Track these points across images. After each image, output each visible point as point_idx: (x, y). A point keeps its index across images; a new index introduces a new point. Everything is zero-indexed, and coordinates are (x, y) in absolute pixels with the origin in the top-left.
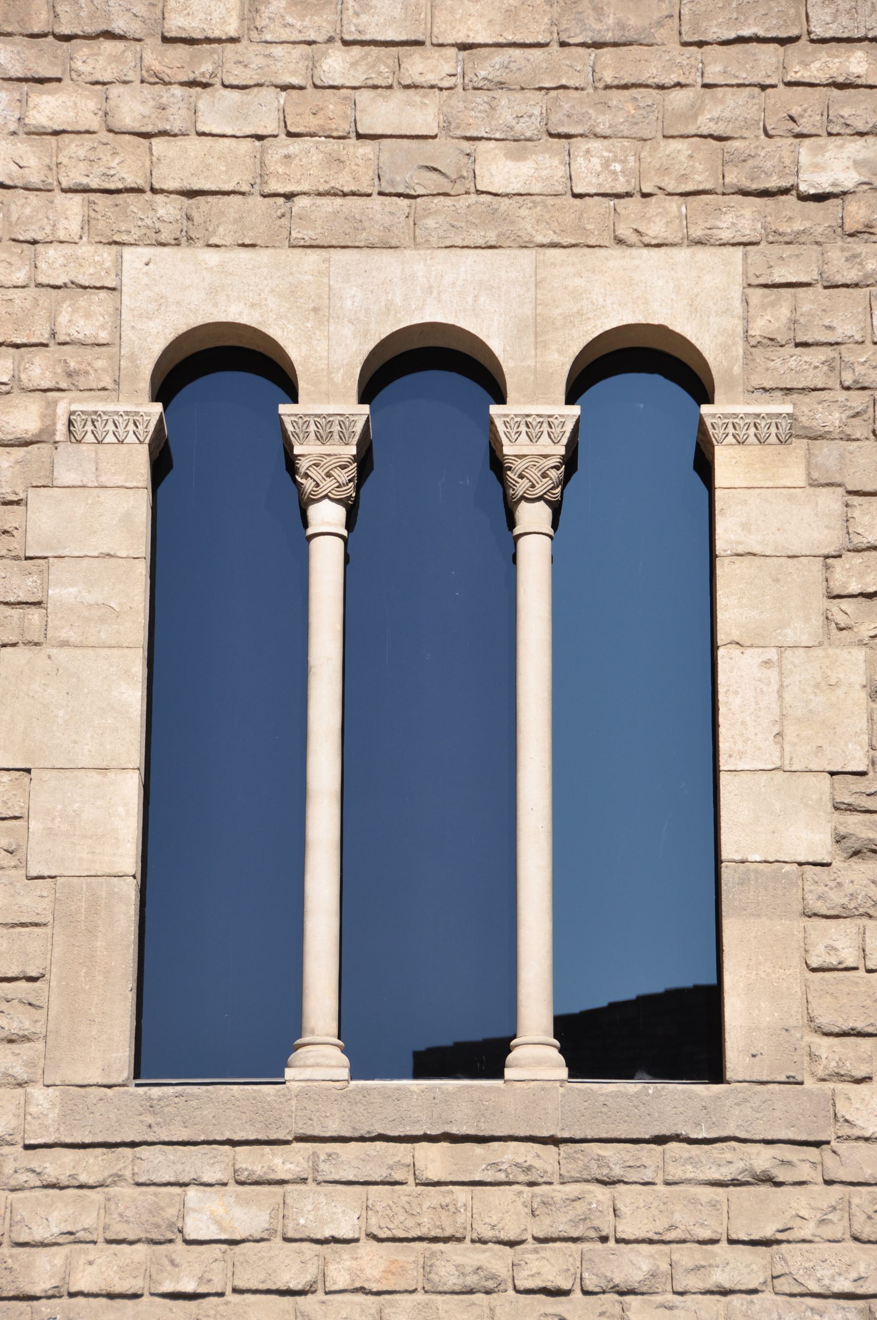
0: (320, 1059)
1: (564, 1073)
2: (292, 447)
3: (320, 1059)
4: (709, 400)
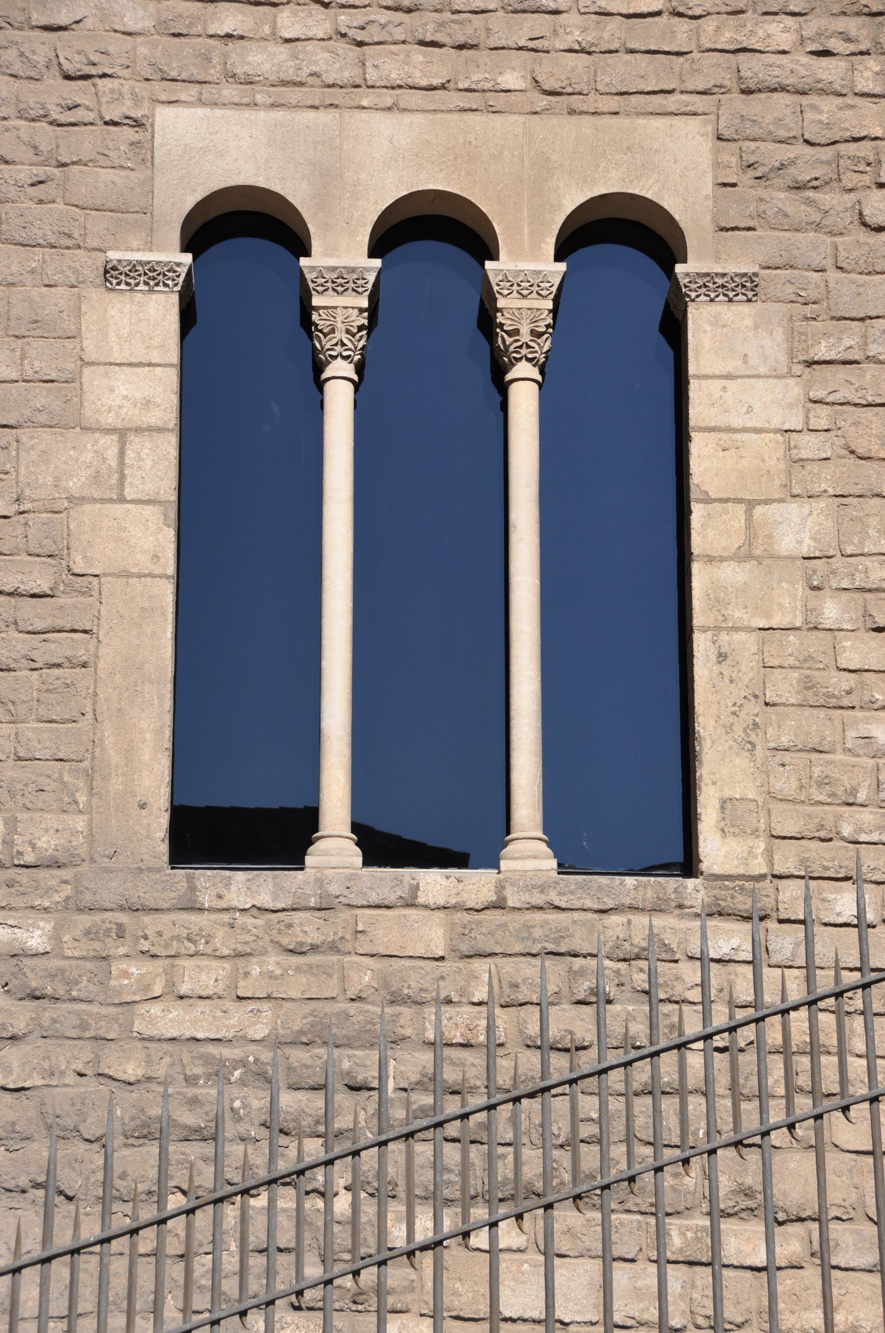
0: (529, 855)
1: (359, 860)
2: (310, 297)
3: (529, 855)
4: (307, 253)
